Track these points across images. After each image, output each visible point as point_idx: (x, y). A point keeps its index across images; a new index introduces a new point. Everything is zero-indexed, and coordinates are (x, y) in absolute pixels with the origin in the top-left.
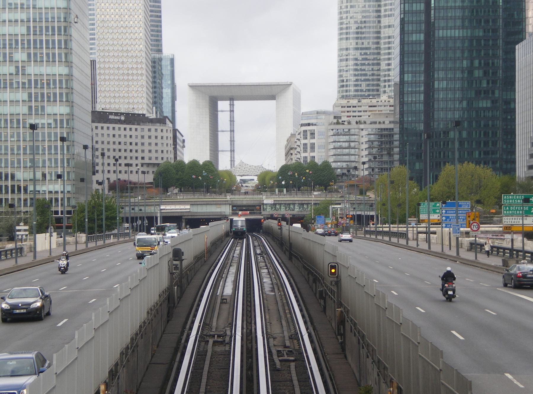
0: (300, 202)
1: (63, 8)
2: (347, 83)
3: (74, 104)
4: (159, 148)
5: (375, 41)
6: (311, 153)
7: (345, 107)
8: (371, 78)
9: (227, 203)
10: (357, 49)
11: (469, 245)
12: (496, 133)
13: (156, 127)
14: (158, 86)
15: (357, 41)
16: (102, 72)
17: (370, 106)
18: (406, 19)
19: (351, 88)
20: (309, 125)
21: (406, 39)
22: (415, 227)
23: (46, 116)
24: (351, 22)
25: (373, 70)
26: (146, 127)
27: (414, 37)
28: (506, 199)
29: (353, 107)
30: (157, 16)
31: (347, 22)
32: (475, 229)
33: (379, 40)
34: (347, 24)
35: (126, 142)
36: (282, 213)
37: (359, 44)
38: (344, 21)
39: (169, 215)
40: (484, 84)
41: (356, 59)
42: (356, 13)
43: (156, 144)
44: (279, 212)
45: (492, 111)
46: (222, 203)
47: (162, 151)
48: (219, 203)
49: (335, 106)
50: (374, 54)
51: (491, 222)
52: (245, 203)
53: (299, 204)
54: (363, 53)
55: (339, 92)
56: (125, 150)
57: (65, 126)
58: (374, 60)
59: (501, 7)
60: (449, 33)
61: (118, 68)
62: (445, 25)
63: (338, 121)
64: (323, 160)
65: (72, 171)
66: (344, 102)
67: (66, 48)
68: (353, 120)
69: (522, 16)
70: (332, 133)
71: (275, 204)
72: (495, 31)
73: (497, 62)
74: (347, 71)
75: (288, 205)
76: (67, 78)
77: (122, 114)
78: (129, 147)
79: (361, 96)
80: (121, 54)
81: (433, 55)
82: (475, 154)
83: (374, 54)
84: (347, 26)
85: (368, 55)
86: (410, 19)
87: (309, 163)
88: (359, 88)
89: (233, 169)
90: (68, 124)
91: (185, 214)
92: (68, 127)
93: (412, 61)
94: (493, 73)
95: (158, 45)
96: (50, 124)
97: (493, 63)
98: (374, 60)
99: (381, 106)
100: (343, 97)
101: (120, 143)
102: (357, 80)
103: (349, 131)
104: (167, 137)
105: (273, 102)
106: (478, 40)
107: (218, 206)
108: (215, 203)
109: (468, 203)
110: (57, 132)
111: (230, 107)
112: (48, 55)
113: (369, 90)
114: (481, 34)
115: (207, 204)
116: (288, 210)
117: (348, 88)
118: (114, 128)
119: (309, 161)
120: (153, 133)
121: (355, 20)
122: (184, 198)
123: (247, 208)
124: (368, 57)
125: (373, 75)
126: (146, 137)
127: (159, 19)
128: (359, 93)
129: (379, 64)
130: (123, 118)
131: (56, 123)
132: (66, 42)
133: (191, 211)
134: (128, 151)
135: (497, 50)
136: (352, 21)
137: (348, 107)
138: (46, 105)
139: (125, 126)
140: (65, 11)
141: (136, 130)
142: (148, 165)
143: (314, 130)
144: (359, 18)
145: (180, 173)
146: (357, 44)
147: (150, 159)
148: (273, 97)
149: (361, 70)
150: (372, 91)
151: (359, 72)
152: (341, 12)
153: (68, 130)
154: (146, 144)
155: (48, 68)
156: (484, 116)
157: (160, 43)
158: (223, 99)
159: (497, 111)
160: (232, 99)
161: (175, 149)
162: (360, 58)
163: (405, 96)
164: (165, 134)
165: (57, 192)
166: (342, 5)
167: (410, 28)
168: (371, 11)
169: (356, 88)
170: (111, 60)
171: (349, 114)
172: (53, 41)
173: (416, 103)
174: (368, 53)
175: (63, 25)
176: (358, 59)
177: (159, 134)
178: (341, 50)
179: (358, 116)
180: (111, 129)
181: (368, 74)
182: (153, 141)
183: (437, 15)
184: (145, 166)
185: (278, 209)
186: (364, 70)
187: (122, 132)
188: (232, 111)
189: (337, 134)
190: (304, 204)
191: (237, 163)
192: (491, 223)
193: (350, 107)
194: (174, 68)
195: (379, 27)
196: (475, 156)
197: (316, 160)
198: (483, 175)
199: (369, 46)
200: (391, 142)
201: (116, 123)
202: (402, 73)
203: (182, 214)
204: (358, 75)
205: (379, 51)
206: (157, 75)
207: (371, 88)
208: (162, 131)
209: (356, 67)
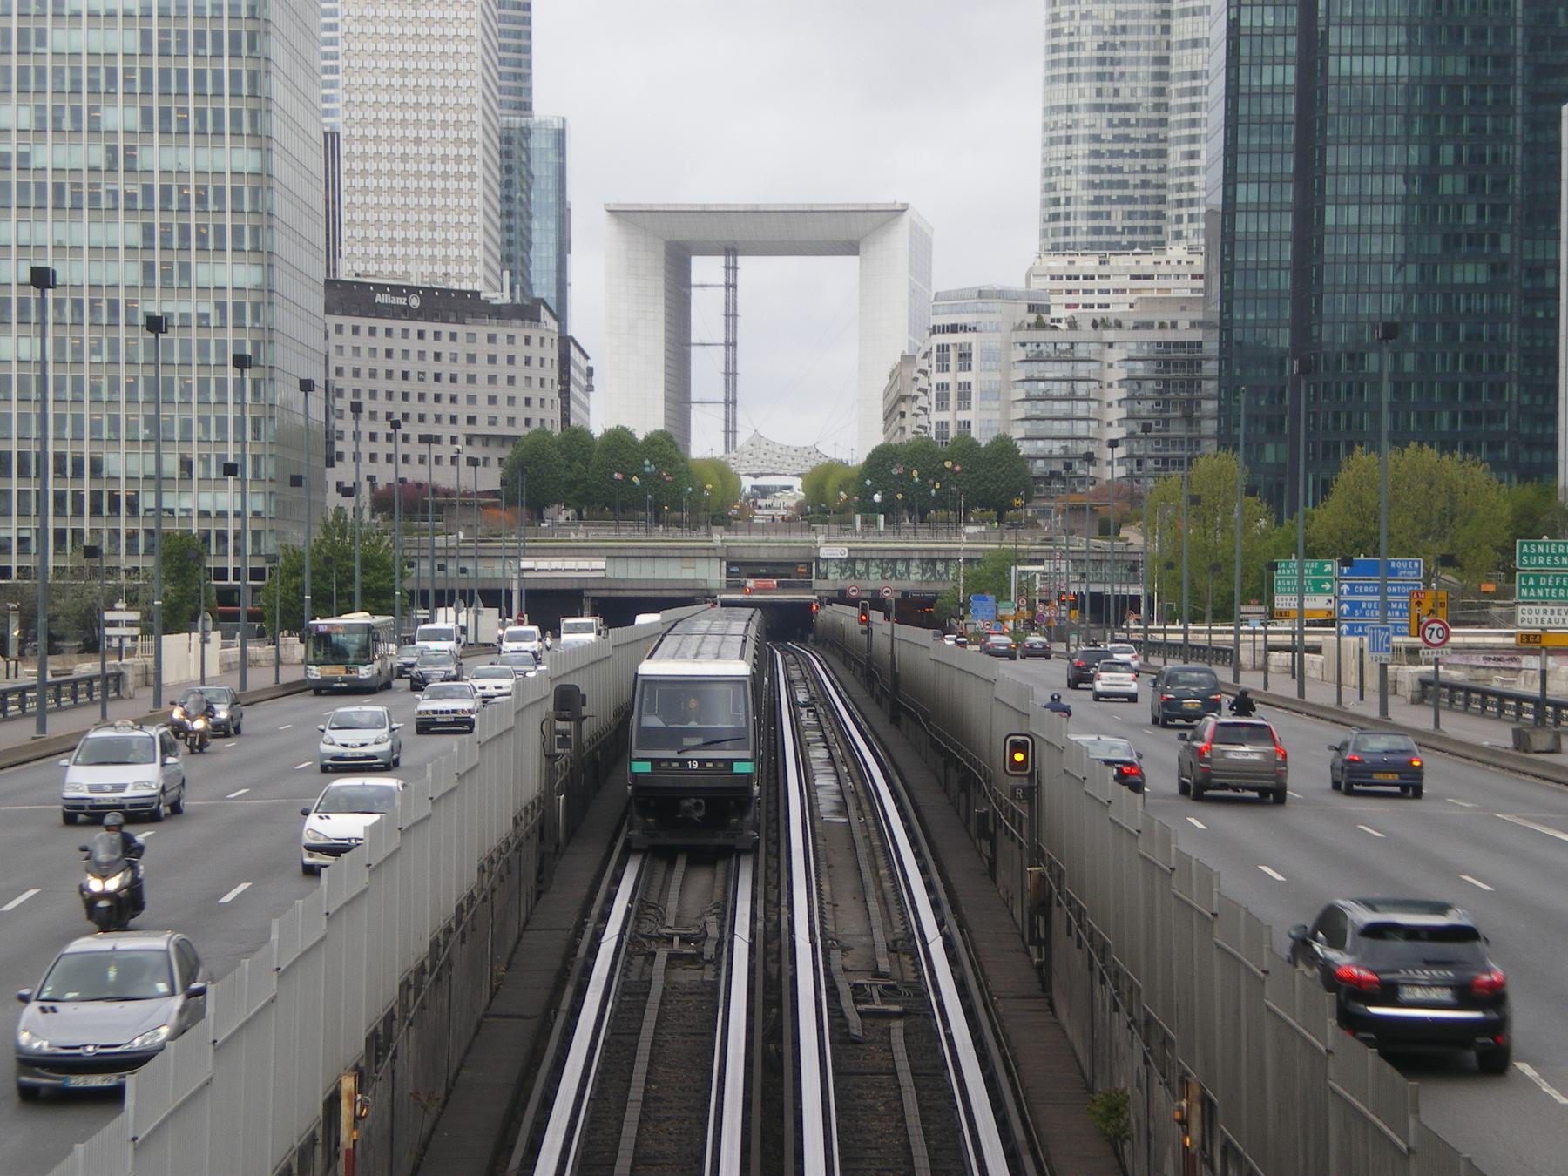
0: (925, 555)
2: (1069, 209)
3: (275, 260)
6: (959, 413)
7: (1060, 278)
8: (1138, 193)
9: (712, 553)
10: (1098, 108)
11: (1417, 687)
13: (511, 331)
14: (518, 208)
15: (1099, 84)
17: (1135, 277)
18: (1245, 22)
19: (1079, 223)
20: (954, 329)
22: (1260, 632)
23: (194, 291)
29: (1085, 278)
31: (1072, 30)
32: (1435, 640)
33: (1163, 84)
34: (1071, 34)
35: (424, 373)
36: (872, 586)
37: (1105, 93)
38: (1064, 24)
41: (1096, 138)
43: (511, 380)
44: (863, 584)
45: (1492, 296)
46: (697, 553)
47: (528, 401)
48: (690, 553)
51: (1483, 619)
52: (764, 555)
53: (921, 559)
55: (1044, 234)
56: (422, 397)
58: (1148, 140)
63: (1039, 318)
65: (267, 454)
66: (1058, 263)
67: (253, 95)
70: (1021, 354)
72: (1503, 62)
73: (1508, 153)
74: (1068, 172)
75: (889, 563)
77: (412, 290)
78: (432, 388)
79: (1110, 246)
81: (1323, 130)
84: (1072, 39)
85: (1132, 126)
87: (955, 442)
88: (1104, 223)
89: (733, 454)
90: (256, 316)
91: (591, 584)
94: (1495, 185)
96: (206, 316)
97: (1496, 156)
98: (1148, 140)
99: (1167, 276)
101: (405, 375)
102: (1098, 200)
103: (1072, 348)
104: (542, 360)
106: (1454, 86)
107: (687, 563)
109: (1416, 565)
111: (727, 275)
113: (1132, 230)
114: (1462, 70)
116: (850, 577)
119: (952, 434)
120: (501, 349)
121: (1096, 23)
123: (771, 570)
124: (1131, 132)
125: (1145, 184)
126: (482, 359)
127: (525, 14)
128: (1105, 238)
129: (1162, 154)
130: (415, 302)
132: (253, 76)
137: (1069, 278)
141: (453, 336)
142: (487, 439)
143: (970, 345)
144: (1107, 17)
146: (1099, 92)
147: (493, 422)
148: (850, 248)
149: (1111, 170)
151: (1103, 177)
153: (257, 336)
156: (1469, 310)
158: (707, 250)
159: (1505, 296)
160: (731, 251)
162: (1108, 134)
165: (222, 515)
169: (1096, 223)
171: (1071, 299)
172: (218, 76)
174: (1133, 121)
175: (245, 27)
176: (1103, 137)
177: (520, 351)
178: (1051, 110)
180: (381, 332)
181: (1131, 182)
182: (502, 370)
184: (477, 443)
185: (902, 575)
186: (1120, 170)
188: (731, 286)
189: (1038, 358)
191: (743, 438)
194: (564, 159)
195: (1164, 44)
197: (975, 434)
200: (1194, 383)
201: (396, 317)
202: (1230, 179)
203: (583, 585)
204: (1100, 185)
205: (1163, 115)
206: (516, 178)
207: (1139, 223)
208: (527, 341)
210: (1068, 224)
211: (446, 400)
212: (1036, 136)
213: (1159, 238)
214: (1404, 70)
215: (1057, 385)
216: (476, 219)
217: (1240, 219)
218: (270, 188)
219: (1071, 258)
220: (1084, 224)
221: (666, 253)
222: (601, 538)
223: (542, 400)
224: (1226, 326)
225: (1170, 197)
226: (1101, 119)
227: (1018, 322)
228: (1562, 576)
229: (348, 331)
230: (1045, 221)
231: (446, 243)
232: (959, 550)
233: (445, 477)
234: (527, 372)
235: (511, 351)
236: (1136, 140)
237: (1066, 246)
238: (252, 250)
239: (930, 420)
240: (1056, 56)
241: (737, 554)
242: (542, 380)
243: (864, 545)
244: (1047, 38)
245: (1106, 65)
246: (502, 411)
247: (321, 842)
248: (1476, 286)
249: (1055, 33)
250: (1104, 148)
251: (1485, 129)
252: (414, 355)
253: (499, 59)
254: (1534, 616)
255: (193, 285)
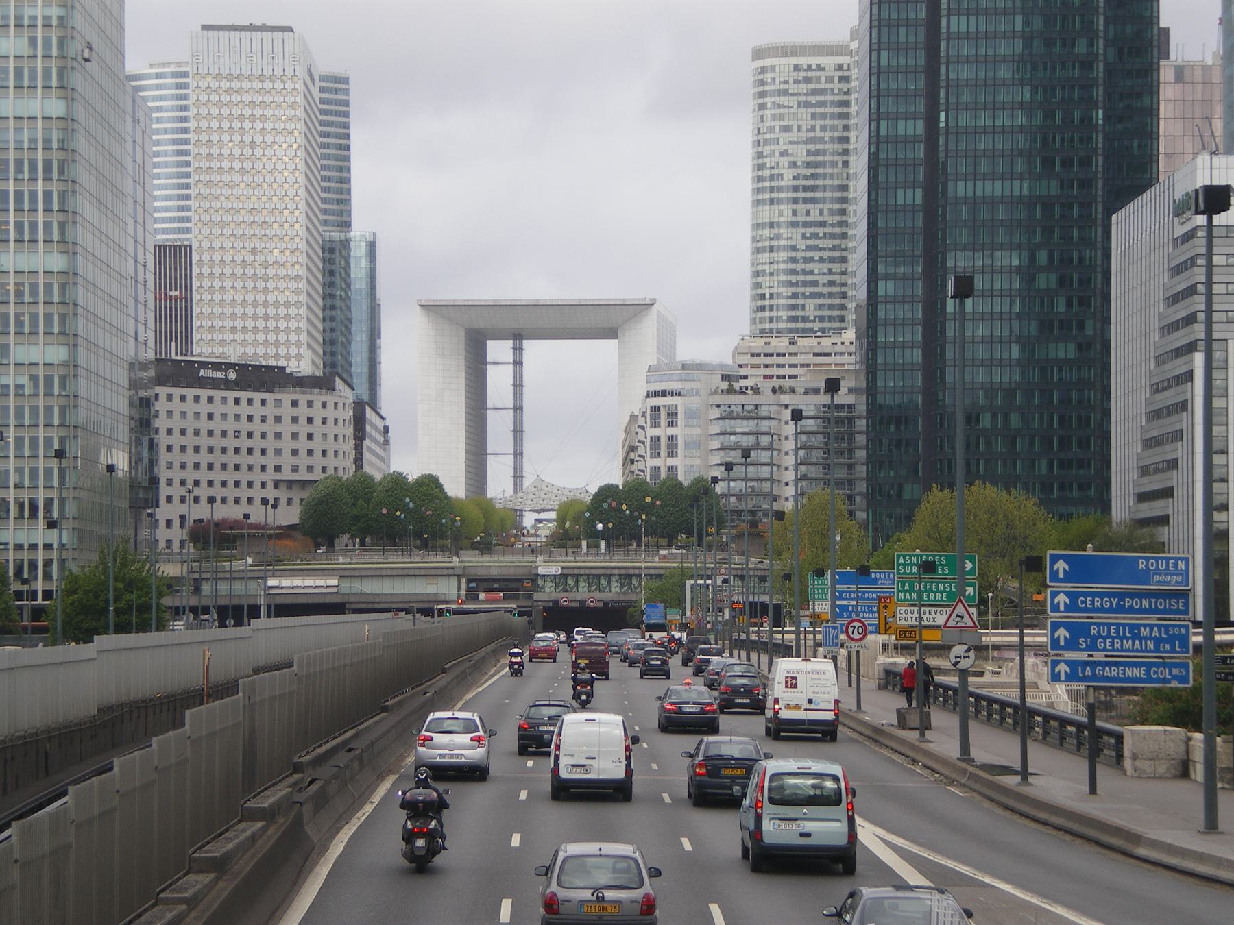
0: (623, 572)
1: (57, 118)
2: (772, 302)
3: (79, 341)
4: (317, 444)
5: (837, 206)
6: (668, 459)
7: (759, 355)
8: (826, 290)
9: (451, 572)
10: (794, 225)
11: (883, 676)
12: (1089, 418)
13: (310, 397)
14: (338, 303)
15: (794, 206)
16: (206, 271)
17: (816, 355)
18: (882, 156)
19: (780, 313)
20: (664, 393)
21: (881, 201)
22: (810, 632)
23: (12, 367)
24: (781, 165)
25: (830, 272)
26: (286, 398)
27: (901, 197)
28: (904, 565)
29: (778, 355)
30: (340, 147)
31: (773, 164)
32: (856, 636)
33: (844, 206)
34: (772, 168)
35: (239, 432)
36: (579, 597)
37: (798, 214)
38: (767, 160)
39: (310, 602)
40: (1061, 307)
41: (794, 248)
42: (793, 143)
43: (310, 436)
44: (571, 595)
45: (1079, 368)
46: (439, 572)
47: (324, 453)
48: (434, 572)
49: (737, 352)
50: (832, 236)
51: (1035, 622)
52: (494, 573)
53: (620, 575)
54: (808, 235)
55: (753, 321)
56: (237, 451)
57: (56, 392)
58: (833, 249)
59: (1100, 128)
60: (981, 188)
61: (244, 264)
62: (988, 169)
63: (730, 385)
64: (696, 475)
65: (71, 497)
66: (758, 344)
67: (62, 210)
68: (766, 386)
69: (1152, 150)
70: (716, 413)
71: (564, 577)
72: (1087, 184)
73: (1091, 258)
74: (771, 274)
75: (594, 578)
76: (63, 279)
77: (230, 366)
78: (245, 443)
79: (797, 330)
80: (249, 231)
81: (944, 239)
82: (1039, 467)
83: (832, 236)
84: (773, 172)
85: (821, 238)
86: (892, 156)
87: (664, 482)
88: (800, 313)
89: (520, 494)
90: (63, 385)
91: (352, 599)
92: (64, 393)
93: (895, 251)
94: (1081, 282)
95: (341, 213)
96: (21, 387)
97: (1081, 259)
98: (833, 249)
99: (842, 354)
100: (762, 333)
101: (224, 434)
102: (795, 296)
103: (756, 409)
104: (336, 420)
105: (611, 345)
106: (1047, 205)
107: (431, 580)
108: (423, 572)
109: (892, 575)
110: (38, 406)
111: (515, 354)
112: (19, 226)
113: (822, 319)
114: (1054, 192)
115: (405, 575)
116: (596, 590)
117: (774, 314)
118: (210, 399)
119: (663, 475)
120: (303, 412)
121: (791, 159)
122: (354, 561)
123: (503, 585)
124: (820, 243)
125: (832, 283)
126: (287, 420)
127: (345, 153)
128: (800, 325)
129: (844, 260)
130: (232, 376)
131: (36, 386)
132: (63, 195)
133: (343, 591)
134: (244, 451)
135: (1090, 227)
136: (784, 161)
137: (766, 355)
138: (12, 344)
139: (237, 394)
140: (61, 124)
141: (263, 402)
142: (290, 484)
143: (676, 406)
144: (799, 154)
145: (361, 502)
146: (794, 213)
147: (295, 469)
148: (611, 333)
149: (805, 272)
150: (830, 321)
151: (798, 278)
152: (759, 141)
153: (63, 402)
154: (287, 436)
155: (19, 256)
156: (1061, 379)
157: (345, 208)
158: (499, 335)
159: (1090, 368)
160: (518, 336)
161: (358, 448)
162: (802, 245)
163: (880, 330)
164: (330, 413)
165: (33, 547)
166: (761, 125)
167: (892, 178)
168: (826, 139)
169: (793, 313)
170: (228, 244)
171: (768, 371)
172: (33, 194)
173: (903, 347)
174: (821, 235)
175: (55, 156)
176: (798, 247)
177: (318, 413)
178: (757, 226)
179: (790, 377)
180: (204, 400)
181: (821, 282)
182: (303, 428)
183: (952, 147)
184: (283, 486)
185: (605, 588)
186: (811, 273)
187: (231, 409)
188: (518, 363)
189: (730, 417)
190: (632, 576)
191: (527, 482)
192: (1036, 626)
193: (772, 355)
194: (375, 265)
195: (845, 175)
196: (1039, 471)
197: (681, 477)
198: (1015, 513)
199: (821, 219)
200: (851, 438)
201: (217, 387)
202: (873, 277)
203: (346, 599)
204: (796, 284)
205: (844, 230)
206: (338, 280)
207: (827, 313)
208: (324, 405)
209: (793, 266)
210: (772, 314)
211: (257, 453)
212: (746, 246)
213: (843, 325)
214: (1026, 192)
215: (745, 437)
216: (301, 312)
217: (881, 308)
218: (75, 284)
219: (767, 340)
220: (784, 314)
221: (467, 339)
222: (363, 561)
223: (336, 452)
224: (871, 390)
225: (850, 293)
226: (797, 234)
227: (714, 388)
228: (932, 583)
229: (176, 399)
230: (754, 312)
231: (277, 330)
232: (640, 568)
233: (258, 515)
234: (323, 429)
235: (310, 413)
236: (824, 249)
237: (771, 331)
238: (60, 334)
239: (648, 464)
240: (760, 185)
241: (472, 572)
242: (336, 436)
243: (574, 564)
244: (753, 170)
245: (805, 192)
246: (303, 461)
247: (1191, 750)
248: (1066, 360)
249: (760, 167)
250: (799, 255)
251: (1072, 238)
252: (231, 418)
253: (321, 187)
254: (909, 615)
255: (12, 362)
